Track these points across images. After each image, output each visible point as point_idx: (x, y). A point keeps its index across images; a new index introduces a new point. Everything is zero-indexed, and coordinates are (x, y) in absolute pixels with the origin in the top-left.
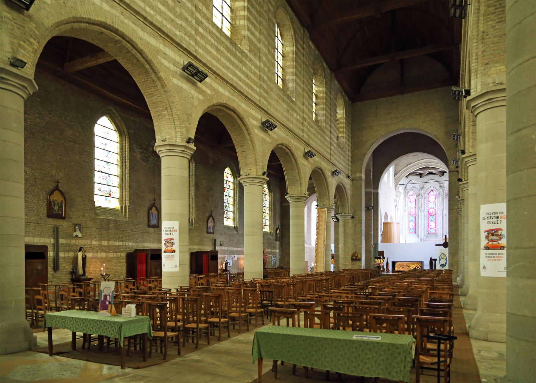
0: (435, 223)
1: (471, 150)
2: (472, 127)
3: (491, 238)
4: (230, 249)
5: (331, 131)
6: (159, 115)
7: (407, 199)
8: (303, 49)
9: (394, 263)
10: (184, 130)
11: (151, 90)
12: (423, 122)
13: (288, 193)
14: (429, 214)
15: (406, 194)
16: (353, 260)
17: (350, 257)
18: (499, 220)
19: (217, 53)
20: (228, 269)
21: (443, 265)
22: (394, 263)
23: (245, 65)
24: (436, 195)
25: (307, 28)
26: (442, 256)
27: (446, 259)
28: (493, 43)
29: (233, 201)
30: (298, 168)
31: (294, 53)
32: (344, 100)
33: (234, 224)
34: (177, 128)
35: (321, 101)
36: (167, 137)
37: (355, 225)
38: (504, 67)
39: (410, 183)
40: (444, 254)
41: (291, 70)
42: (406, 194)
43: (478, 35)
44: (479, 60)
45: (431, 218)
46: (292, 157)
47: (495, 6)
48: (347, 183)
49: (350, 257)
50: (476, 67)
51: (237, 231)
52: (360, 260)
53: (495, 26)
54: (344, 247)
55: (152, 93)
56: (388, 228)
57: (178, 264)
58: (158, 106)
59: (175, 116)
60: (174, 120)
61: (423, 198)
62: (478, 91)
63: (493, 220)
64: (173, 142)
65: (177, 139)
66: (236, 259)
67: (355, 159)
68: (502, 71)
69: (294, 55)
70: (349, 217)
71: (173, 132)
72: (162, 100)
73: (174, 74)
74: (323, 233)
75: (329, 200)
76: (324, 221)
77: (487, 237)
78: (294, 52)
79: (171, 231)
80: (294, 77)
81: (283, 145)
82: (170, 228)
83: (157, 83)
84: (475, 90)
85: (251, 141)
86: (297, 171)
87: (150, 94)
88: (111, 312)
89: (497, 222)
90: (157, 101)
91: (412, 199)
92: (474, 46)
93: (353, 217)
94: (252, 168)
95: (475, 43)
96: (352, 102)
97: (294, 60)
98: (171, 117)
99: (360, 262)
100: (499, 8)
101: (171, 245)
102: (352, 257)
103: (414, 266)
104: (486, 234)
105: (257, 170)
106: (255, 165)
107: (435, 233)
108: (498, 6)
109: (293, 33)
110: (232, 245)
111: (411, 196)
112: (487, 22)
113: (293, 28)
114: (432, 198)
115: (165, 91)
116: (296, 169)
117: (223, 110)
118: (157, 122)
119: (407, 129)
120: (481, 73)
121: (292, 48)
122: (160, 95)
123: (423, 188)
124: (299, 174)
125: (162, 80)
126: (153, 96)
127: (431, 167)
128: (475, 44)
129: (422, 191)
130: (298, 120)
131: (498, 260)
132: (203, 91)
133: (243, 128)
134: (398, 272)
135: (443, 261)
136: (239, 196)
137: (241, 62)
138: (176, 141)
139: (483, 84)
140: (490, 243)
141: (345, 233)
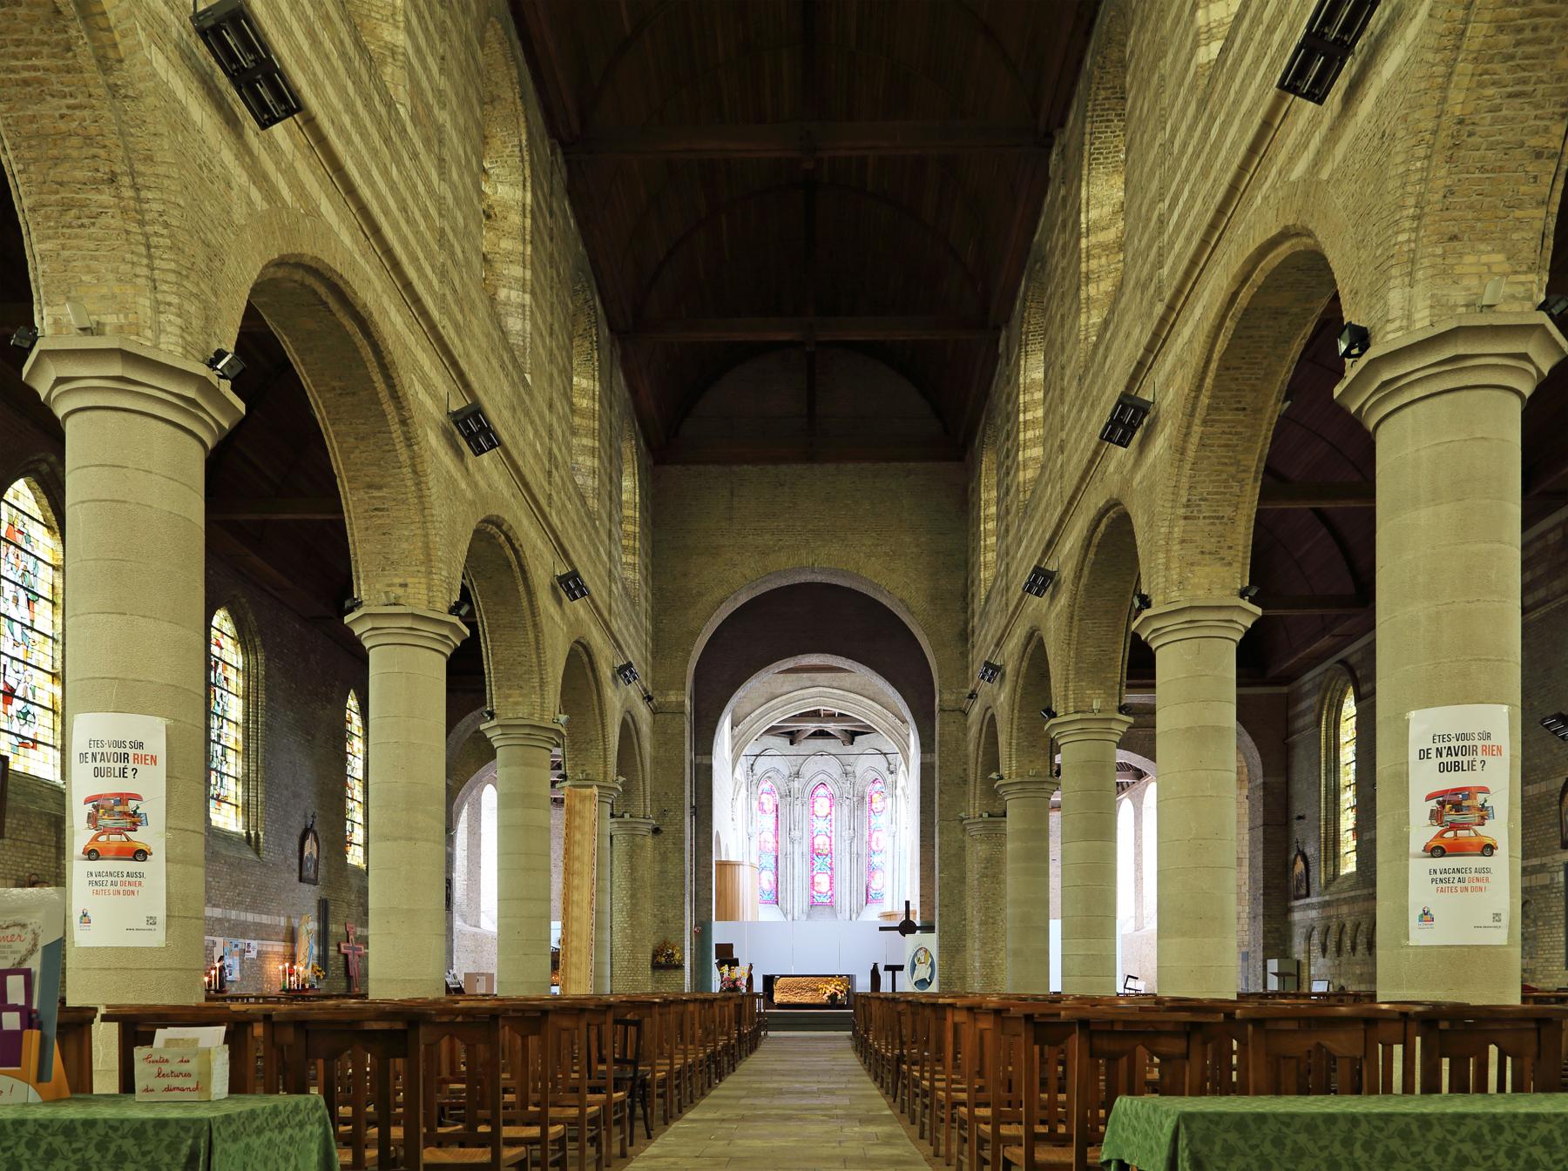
0: (831, 878)
1: (1175, 595)
2: (1182, 522)
3: (1451, 816)
4: (233, 914)
5: (610, 531)
6: (66, 207)
7: (755, 804)
8: (552, 214)
9: (769, 981)
10: (192, 308)
11: (35, 62)
12: (868, 556)
13: (492, 715)
14: (815, 852)
15: (754, 787)
16: (656, 966)
17: (646, 958)
18: (1479, 758)
19: (311, 45)
20: (228, 986)
21: (923, 983)
22: (769, 981)
23: (399, 163)
24: (832, 798)
25: (563, 144)
26: (921, 955)
27: (932, 965)
28: (1482, 170)
29: (240, 737)
30: (535, 625)
31: (529, 215)
32: (637, 445)
33: (247, 826)
34: (165, 287)
35: (585, 422)
36: (110, 320)
37: (664, 858)
38: (1500, 257)
39: (767, 752)
40: (926, 951)
41: (516, 271)
42: (754, 787)
43: (1434, 133)
44: (1426, 220)
45: (818, 861)
46: (520, 582)
47: (1520, 30)
48: (643, 712)
49: (649, 957)
50: (1413, 245)
51: (257, 851)
52: (680, 967)
53: (1498, 109)
54: (632, 925)
55: (39, 81)
56: (728, 878)
57: (161, 915)
58: (67, 158)
59: (158, 228)
60: (148, 247)
61: (798, 802)
62: (1418, 325)
63: (1460, 758)
64: (142, 345)
65: (163, 338)
66: (253, 954)
67: (662, 645)
68: (1495, 269)
69: (528, 221)
70: (645, 829)
71: (145, 302)
72: (93, 130)
73: (159, 34)
74: (587, 869)
75: (605, 761)
76: (587, 829)
77: (1436, 816)
78: (528, 208)
79: (125, 757)
80: (527, 297)
81: (499, 526)
82: (121, 744)
83: (73, 33)
84: (1405, 323)
85: (415, 472)
86: (531, 636)
87: (26, 83)
88: (42, 1075)
89: (1471, 766)
90: (62, 126)
91: (769, 806)
92: (1417, 170)
93: (656, 831)
94: (409, 580)
95: (1419, 159)
96: (656, 463)
97: (528, 237)
98: (133, 227)
99: (678, 973)
100: (1529, 42)
101: (125, 823)
102: (654, 956)
103: (830, 989)
104: (1433, 804)
105: (429, 589)
106: (423, 569)
107: (831, 905)
108: (1528, 34)
109: (524, 137)
110: (240, 903)
111: (764, 796)
112: (1481, 85)
113: (527, 120)
114: (822, 806)
115: (113, 89)
116: (530, 628)
117: (325, 304)
118: (55, 236)
119: (822, 571)
120: (1433, 266)
121: (519, 194)
122: (80, 99)
123: (797, 774)
124: (538, 648)
125: (101, 22)
126: (40, 99)
127: (840, 715)
128: (1419, 164)
129: (796, 784)
130: (536, 455)
131: (1474, 889)
132: (266, 177)
133: (389, 407)
134: (781, 1006)
135: (923, 972)
136: (266, 724)
137: (387, 140)
138: (156, 346)
139: (1438, 304)
140: (1450, 834)
141: (633, 880)
